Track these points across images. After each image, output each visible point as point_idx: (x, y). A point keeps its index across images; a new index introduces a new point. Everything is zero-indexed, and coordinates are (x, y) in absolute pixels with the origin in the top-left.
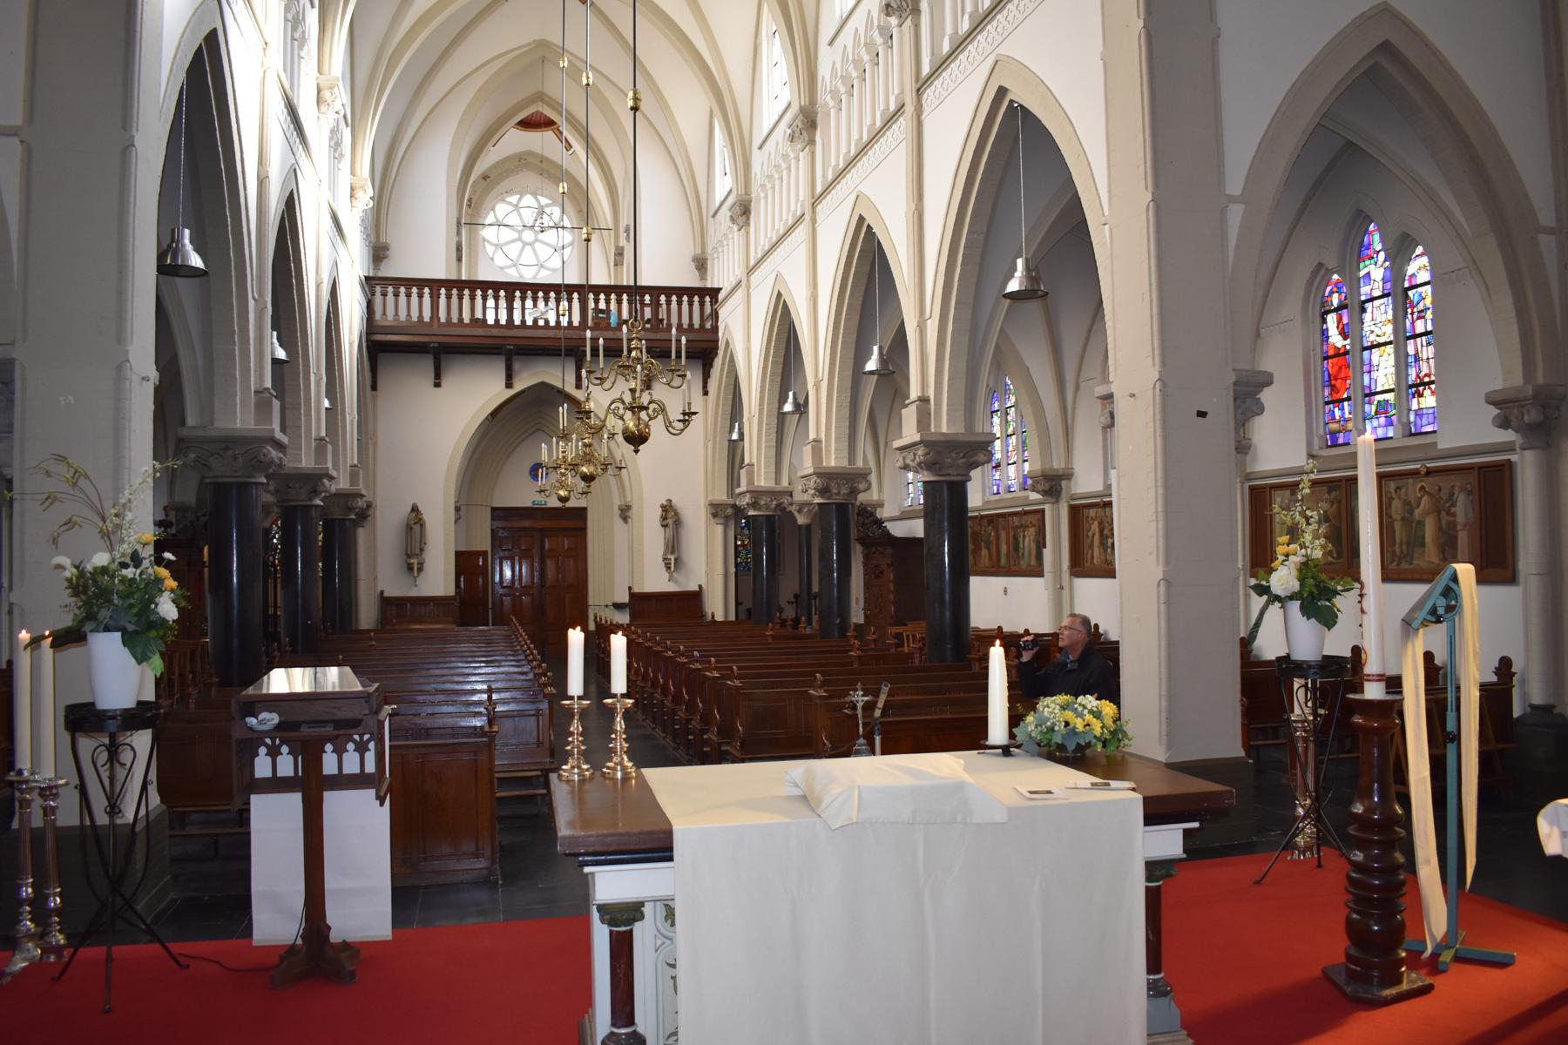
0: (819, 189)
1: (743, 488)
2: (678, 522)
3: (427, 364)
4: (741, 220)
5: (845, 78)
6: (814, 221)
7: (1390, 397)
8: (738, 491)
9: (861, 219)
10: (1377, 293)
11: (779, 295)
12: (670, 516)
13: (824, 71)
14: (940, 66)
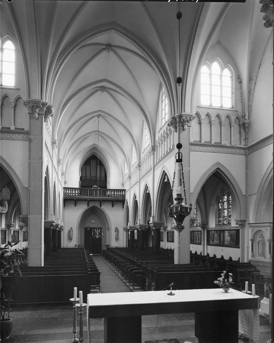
0: (141, 178)
1: (138, 224)
2: (118, 231)
3: (73, 202)
4: (129, 179)
5: (161, 140)
6: (140, 183)
7: (226, 217)
8: (128, 226)
9: (164, 171)
10: (226, 201)
11: (146, 185)
12: (117, 230)
13: (142, 157)
14: (157, 164)
